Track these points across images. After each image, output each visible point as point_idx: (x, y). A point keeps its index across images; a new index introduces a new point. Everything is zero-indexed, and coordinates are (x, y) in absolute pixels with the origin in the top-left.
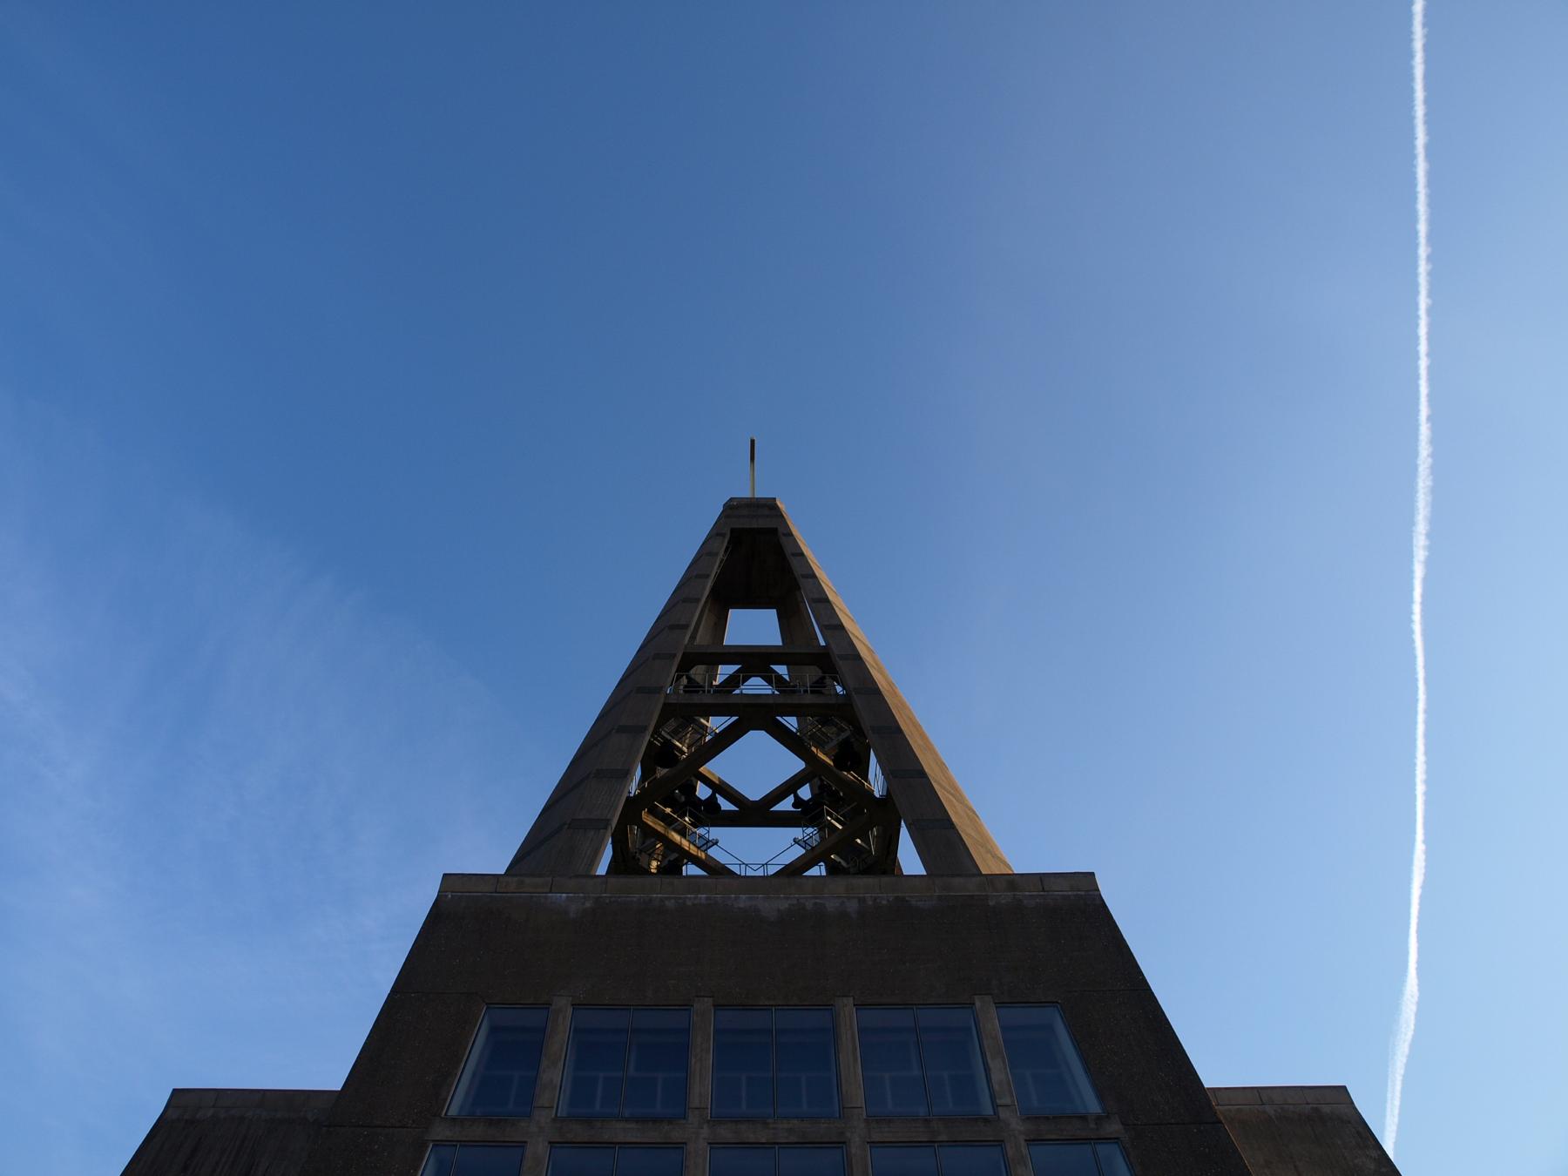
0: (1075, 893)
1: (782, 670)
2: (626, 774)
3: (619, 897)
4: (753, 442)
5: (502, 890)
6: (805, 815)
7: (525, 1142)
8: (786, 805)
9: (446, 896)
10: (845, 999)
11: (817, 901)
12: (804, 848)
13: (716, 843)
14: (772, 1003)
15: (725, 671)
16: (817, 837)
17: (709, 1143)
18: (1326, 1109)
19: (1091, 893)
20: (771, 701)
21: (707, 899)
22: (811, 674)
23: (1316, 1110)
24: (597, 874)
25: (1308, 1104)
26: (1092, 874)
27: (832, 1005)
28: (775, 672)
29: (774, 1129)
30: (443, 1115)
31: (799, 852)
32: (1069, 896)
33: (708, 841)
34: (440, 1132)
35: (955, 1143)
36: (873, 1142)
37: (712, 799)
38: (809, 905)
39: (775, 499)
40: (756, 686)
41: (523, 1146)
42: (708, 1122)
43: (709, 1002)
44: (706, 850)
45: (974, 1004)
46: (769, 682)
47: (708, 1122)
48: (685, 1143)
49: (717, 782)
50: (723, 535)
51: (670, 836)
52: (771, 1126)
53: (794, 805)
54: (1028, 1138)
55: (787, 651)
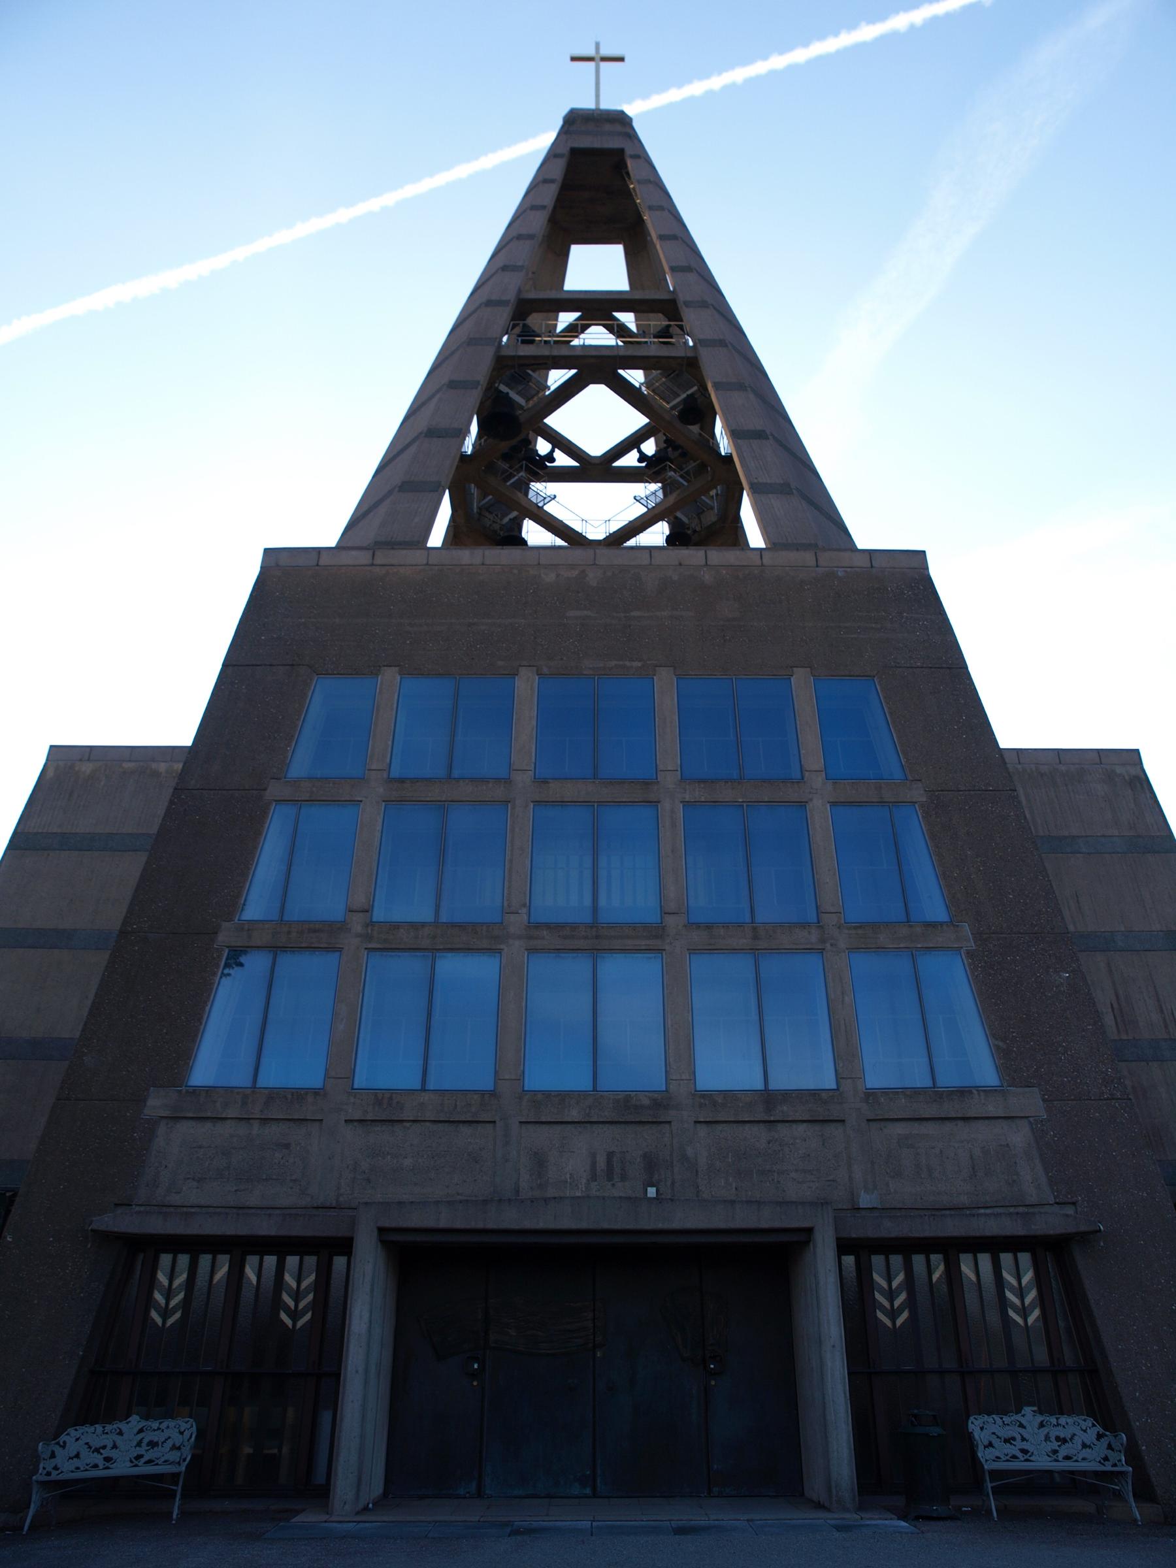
1: (628, 319)
2: (465, 432)
6: (649, 470)
7: (342, 948)
8: (630, 460)
12: (647, 507)
15: (566, 319)
16: (660, 494)
20: (615, 353)
22: (658, 321)
24: (295, 1289)
26: (924, 552)
28: (616, 319)
40: (597, 336)
41: (341, 951)
46: (610, 329)
50: (552, 181)
53: (640, 461)
55: (637, 297)
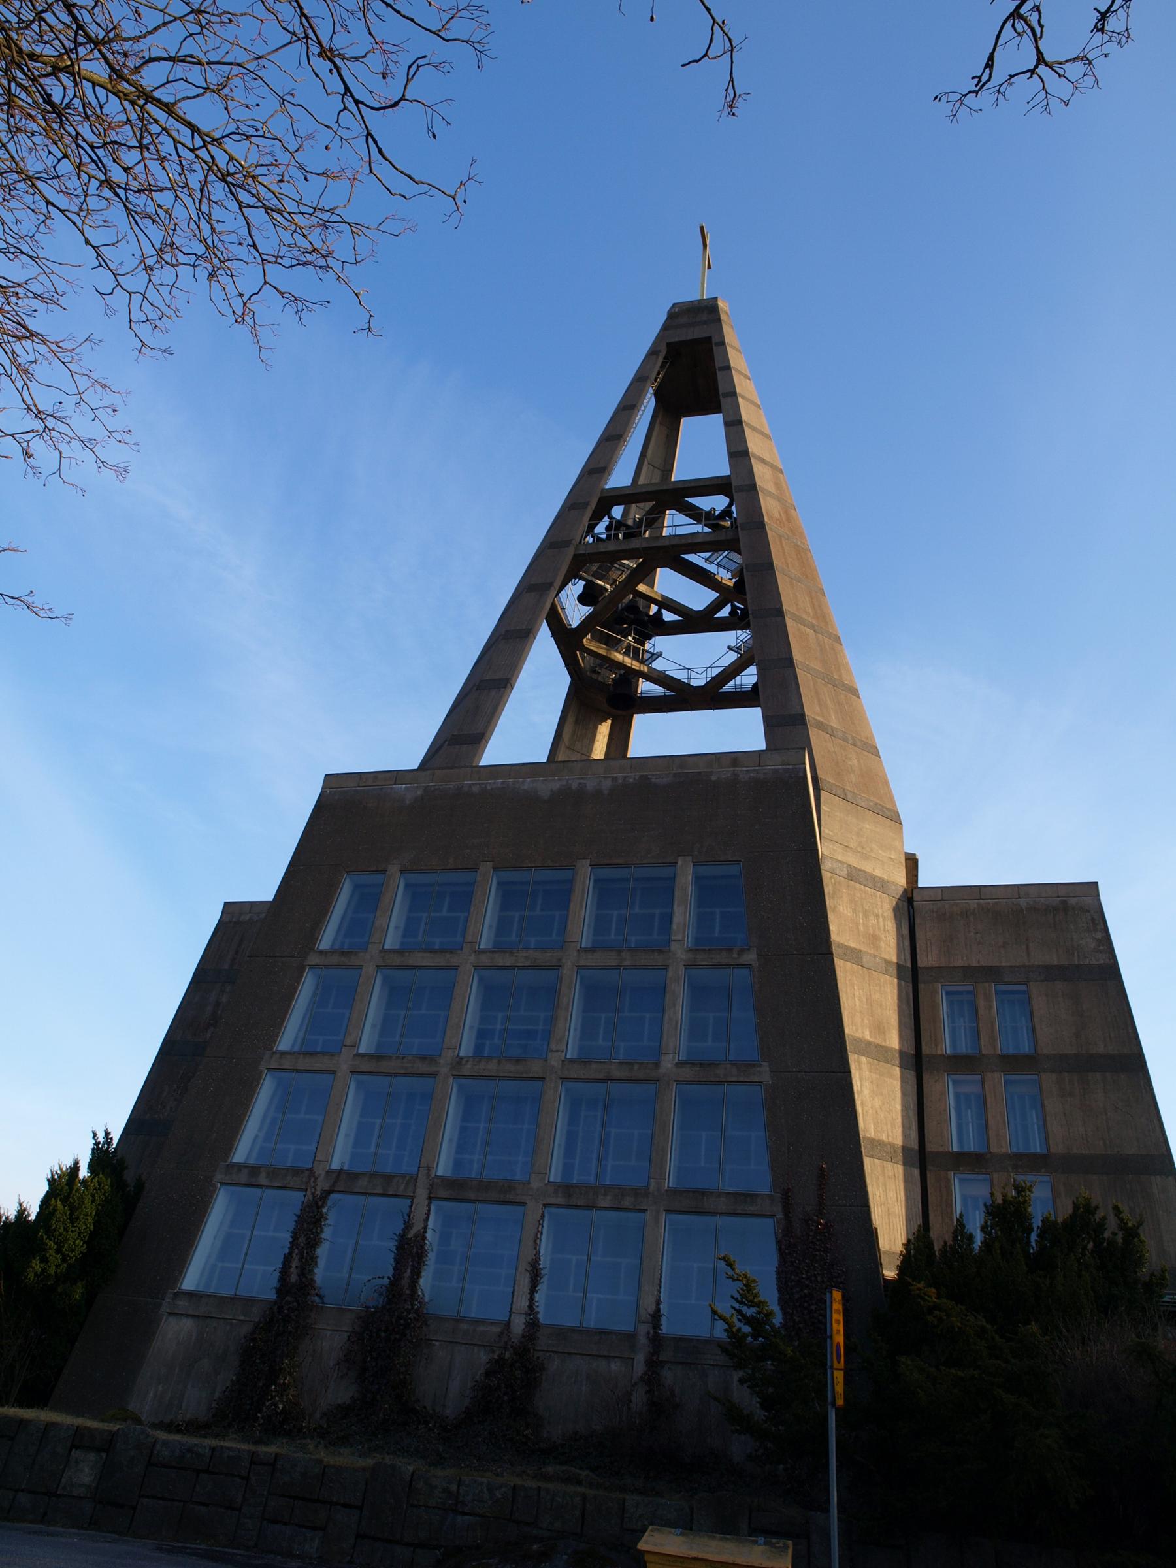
0: (784, 767)
3: (441, 785)
4: (702, 228)
5: (364, 785)
7: (362, 966)
9: (326, 791)
10: (584, 860)
11: (582, 781)
13: (660, 655)
14: (533, 865)
17: (474, 966)
18: (1073, 901)
19: (797, 766)
21: (503, 783)
23: (1064, 902)
25: (1058, 897)
27: (574, 866)
29: (516, 956)
30: (316, 948)
31: (733, 656)
32: (779, 769)
33: (653, 654)
34: (313, 959)
35: (635, 967)
36: (579, 966)
37: (659, 613)
38: (574, 785)
39: (716, 299)
42: (475, 952)
43: (490, 865)
44: (651, 663)
45: (677, 863)
47: (475, 952)
48: (459, 966)
49: (660, 599)
51: (612, 657)
52: (516, 954)
54: (686, 964)
